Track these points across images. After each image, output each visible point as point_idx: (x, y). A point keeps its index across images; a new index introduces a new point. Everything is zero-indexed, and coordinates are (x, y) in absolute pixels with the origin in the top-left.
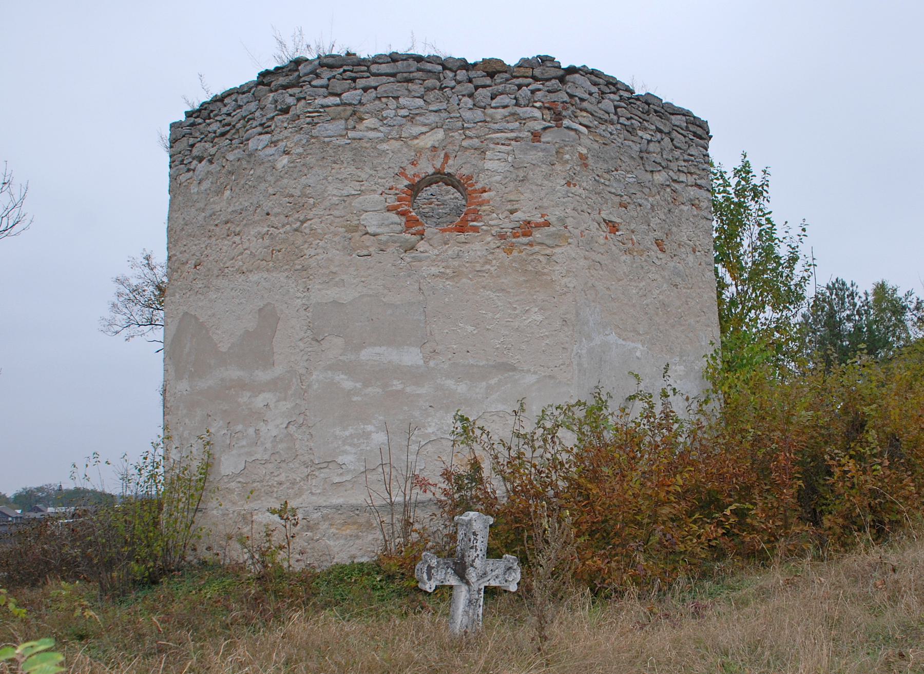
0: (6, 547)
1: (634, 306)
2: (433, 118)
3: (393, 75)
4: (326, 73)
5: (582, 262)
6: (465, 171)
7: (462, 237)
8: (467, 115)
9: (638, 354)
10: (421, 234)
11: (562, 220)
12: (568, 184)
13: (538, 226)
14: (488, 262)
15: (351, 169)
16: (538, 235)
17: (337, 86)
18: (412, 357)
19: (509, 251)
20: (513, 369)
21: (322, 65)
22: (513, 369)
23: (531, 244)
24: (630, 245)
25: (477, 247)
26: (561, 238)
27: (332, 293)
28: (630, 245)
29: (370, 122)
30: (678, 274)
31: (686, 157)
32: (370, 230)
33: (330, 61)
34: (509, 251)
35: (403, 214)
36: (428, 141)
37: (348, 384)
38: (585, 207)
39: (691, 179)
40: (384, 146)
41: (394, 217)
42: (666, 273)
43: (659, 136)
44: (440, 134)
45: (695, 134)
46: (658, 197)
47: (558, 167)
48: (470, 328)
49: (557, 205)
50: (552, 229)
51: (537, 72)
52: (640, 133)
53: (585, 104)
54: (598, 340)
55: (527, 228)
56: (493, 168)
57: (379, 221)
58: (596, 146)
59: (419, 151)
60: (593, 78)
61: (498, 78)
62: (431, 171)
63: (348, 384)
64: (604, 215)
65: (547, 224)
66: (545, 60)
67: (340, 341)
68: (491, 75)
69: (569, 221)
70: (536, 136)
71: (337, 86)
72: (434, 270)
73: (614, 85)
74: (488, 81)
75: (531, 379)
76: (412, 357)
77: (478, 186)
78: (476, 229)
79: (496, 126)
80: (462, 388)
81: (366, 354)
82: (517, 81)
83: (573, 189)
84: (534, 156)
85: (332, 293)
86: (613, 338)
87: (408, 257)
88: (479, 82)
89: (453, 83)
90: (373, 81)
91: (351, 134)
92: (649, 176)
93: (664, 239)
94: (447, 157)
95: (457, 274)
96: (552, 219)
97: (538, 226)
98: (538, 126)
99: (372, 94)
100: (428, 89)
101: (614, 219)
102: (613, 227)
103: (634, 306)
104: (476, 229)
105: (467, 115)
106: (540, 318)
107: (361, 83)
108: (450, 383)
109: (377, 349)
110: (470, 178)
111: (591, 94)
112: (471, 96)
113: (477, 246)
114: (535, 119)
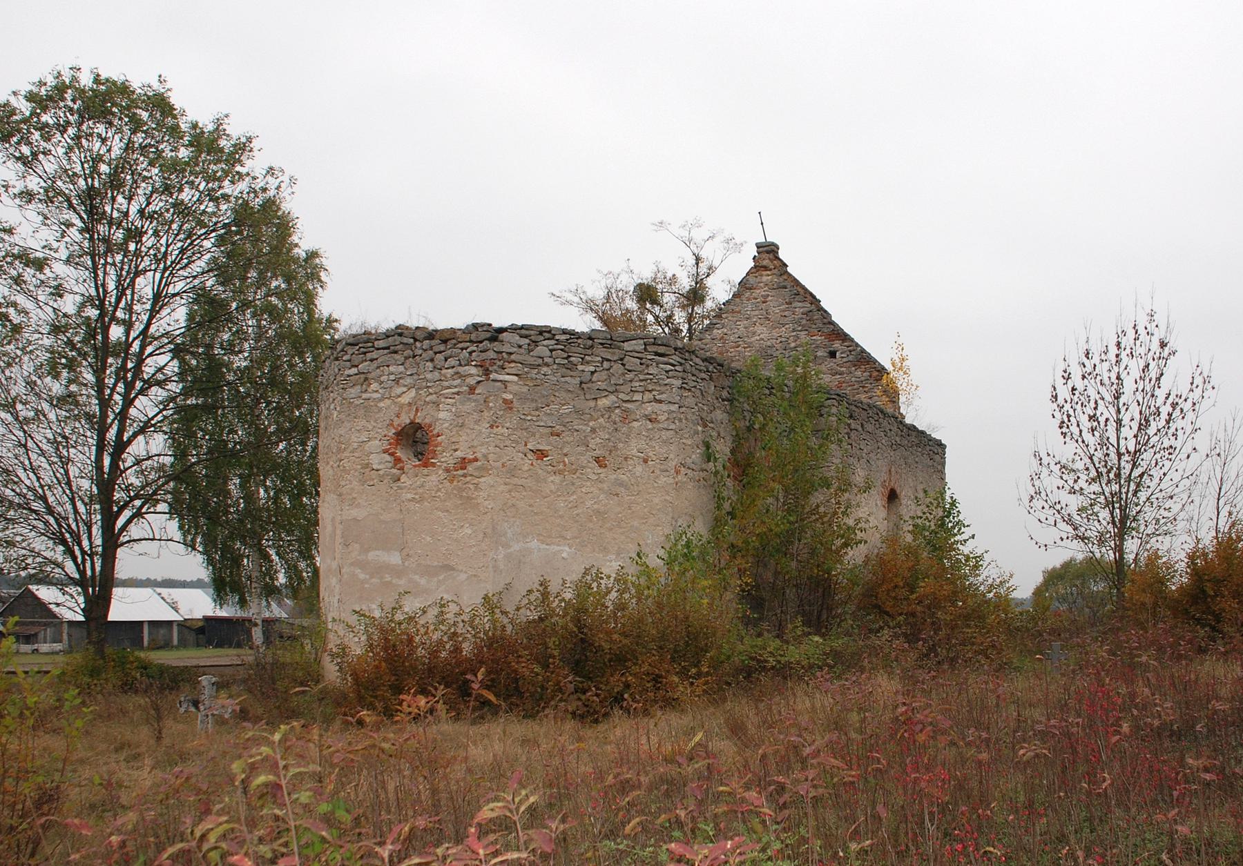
0: (5, 592)
1: (561, 517)
2: (409, 381)
3: (388, 348)
4: (350, 350)
5: (502, 488)
6: (427, 421)
7: (426, 471)
8: (429, 376)
9: (564, 555)
10: (402, 469)
11: (485, 456)
12: (492, 427)
13: (471, 461)
14: (439, 490)
15: (364, 422)
16: (470, 468)
17: (356, 359)
18: (395, 559)
19: (451, 482)
20: (453, 569)
21: (348, 344)
22: (453, 569)
23: (465, 476)
24: (561, 466)
25: (434, 478)
26: (484, 470)
27: (354, 513)
28: (561, 466)
29: (374, 386)
30: (621, 485)
31: (642, 377)
32: (375, 467)
33: (351, 340)
34: (451, 482)
35: (392, 454)
36: (405, 399)
37: (362, 576)
38: (508, 443)
39: (648, 396)
40: (381, 404)
41: (388, 458)
42: (605, 486)
43: (606, 364)
44: (413, 393)
45: (657, 354)
46: (601, 420)
47: (486, 414)
48: (429, 539)
49: (482, 445)
50: (479, 463)
51: (473, 337)
52: (580, 367)
53: (513, 357)
54: (516, 547)
55: (463, 463)
56: (442, 418)
57: (380, 461)
58: (525, 389)
59: (402, 406)
60: (523, 332)
61: (450, 344)
62: (408, 421)
63: (362, 576)
64: (530, 446)
65: (476, 460)
66: (475, 326)
67: (357, 546)
68: (445, 342)
69: (491, 457)
70: (472, 389)
71: (356, 359)
72: (409, 496)
73: (549, 332)
74: (442, 348)
75: (463, 577)
76: (395, 559)
77: (435, 432)
78: (433, 465)
79: (446, 384)
80: (423, 581)
81: (372, 555)
82: (460, 345)
83: (495, 430)
84: (469, 406)
85: (354, 513)
86: (534, 544)
87: (395, 486)
88: (436, 349)
89: (420, 352)
90: (374, 355)
91: (364, 396)
92: (592, 404)
93: (607, 455)
94: (417, 410)
95: (422, 499)
96: (479, 455)
97: (471, 461)
98: (472, 381)
99: (375, 364)
100: (406, 358)
101: (541, 448)
102: (541, 454)
103: (561, 517)
104: (433, 465)
105: (429, 376)
106: (469, 532)
107: (369, 356)
108: (417, 577)
109: (377, 553)
110: (430, 426)
111: (520, 347)
112: (432, 360)
113: (433, 478)
114: (471, 375)
